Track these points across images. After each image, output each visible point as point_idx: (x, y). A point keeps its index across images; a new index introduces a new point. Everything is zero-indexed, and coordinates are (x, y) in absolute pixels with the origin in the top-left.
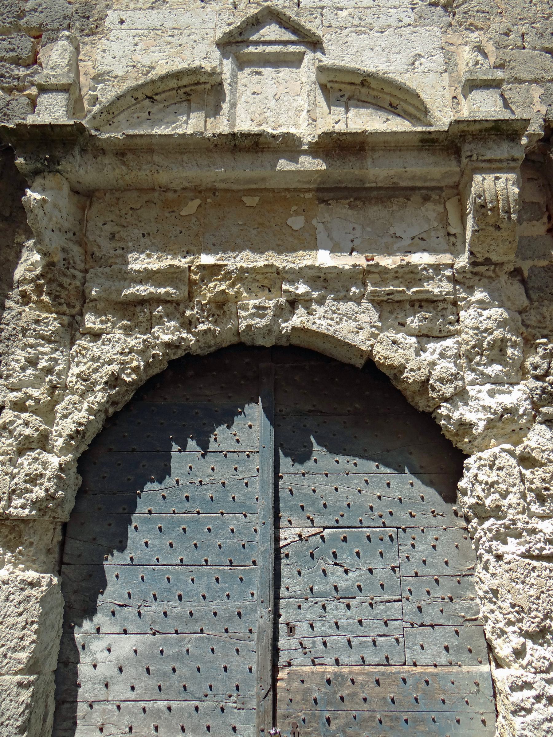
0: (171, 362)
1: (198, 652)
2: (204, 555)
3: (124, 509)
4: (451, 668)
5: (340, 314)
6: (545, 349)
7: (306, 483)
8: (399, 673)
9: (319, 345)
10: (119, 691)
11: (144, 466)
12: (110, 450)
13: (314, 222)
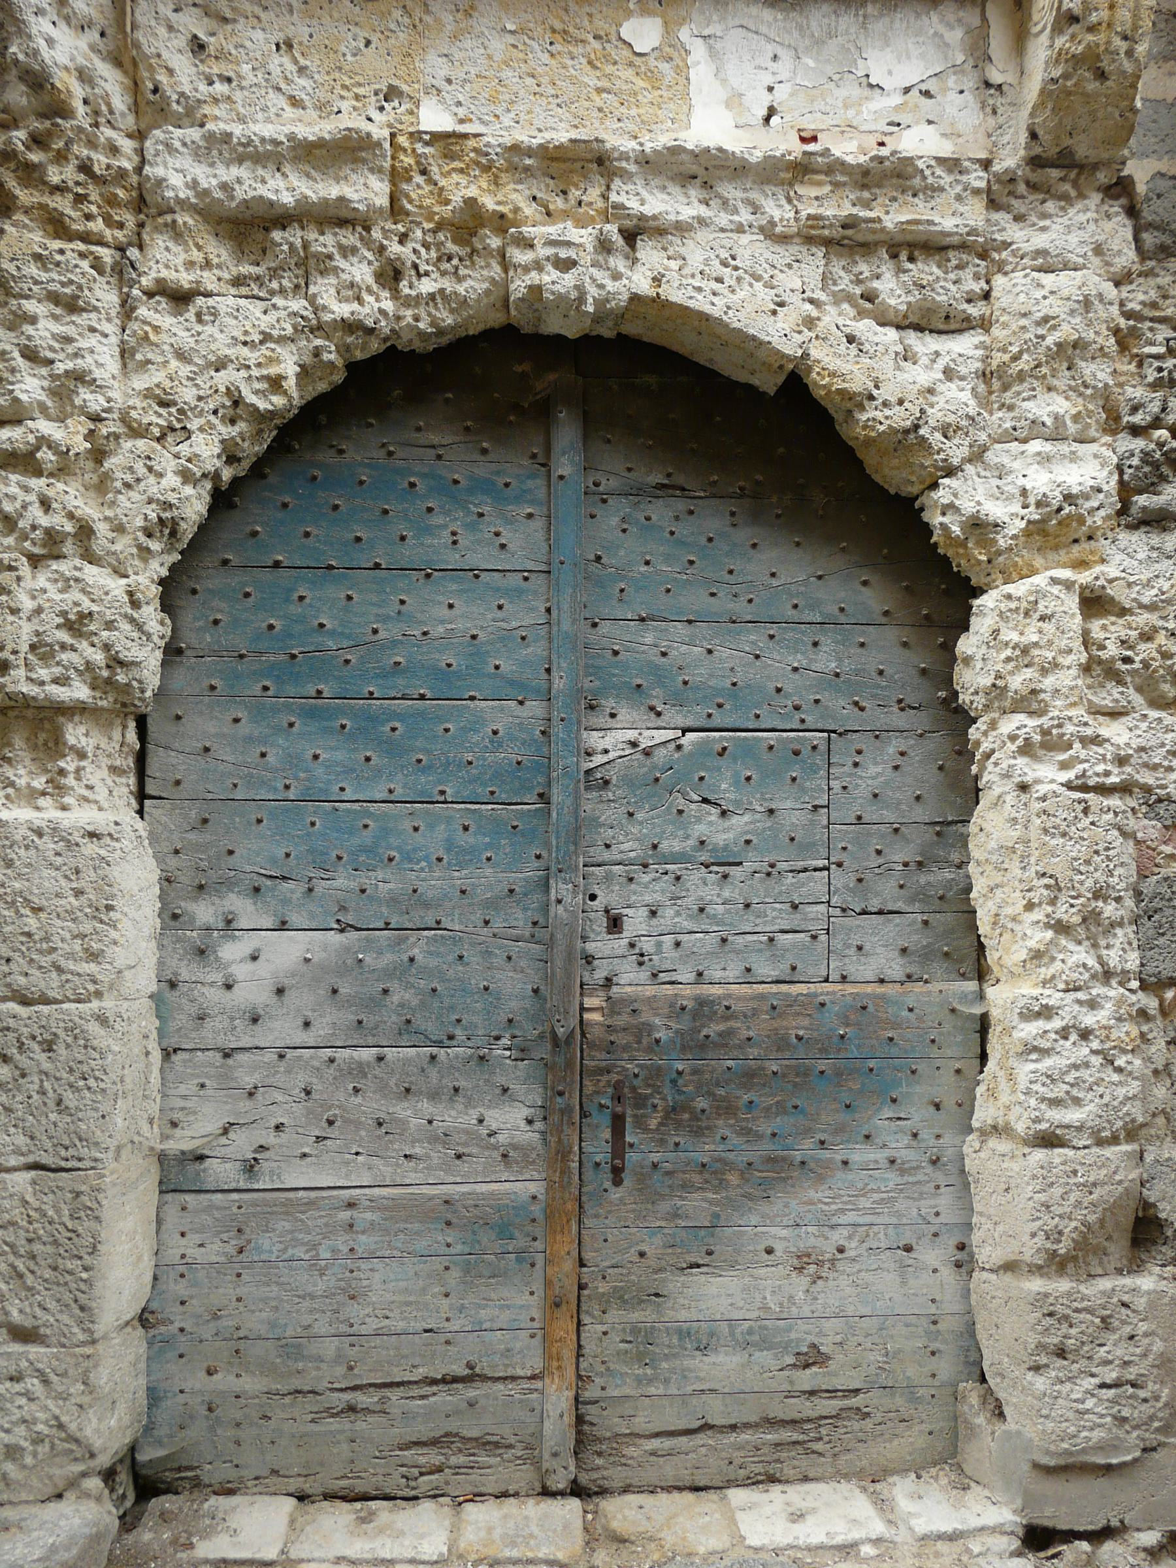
0: (351, 367)
1: (433, 962)
2: (440, 782)
3: (266, 688)
4: (909, 986)
5: (736, 268)
6: (1160, 370)
7: (649, 639)
8: (816, 995)
9: (685, 343)
10: (281, 1029)
11: (301, 598)
12: (225, 562)
13: (684, 34)
